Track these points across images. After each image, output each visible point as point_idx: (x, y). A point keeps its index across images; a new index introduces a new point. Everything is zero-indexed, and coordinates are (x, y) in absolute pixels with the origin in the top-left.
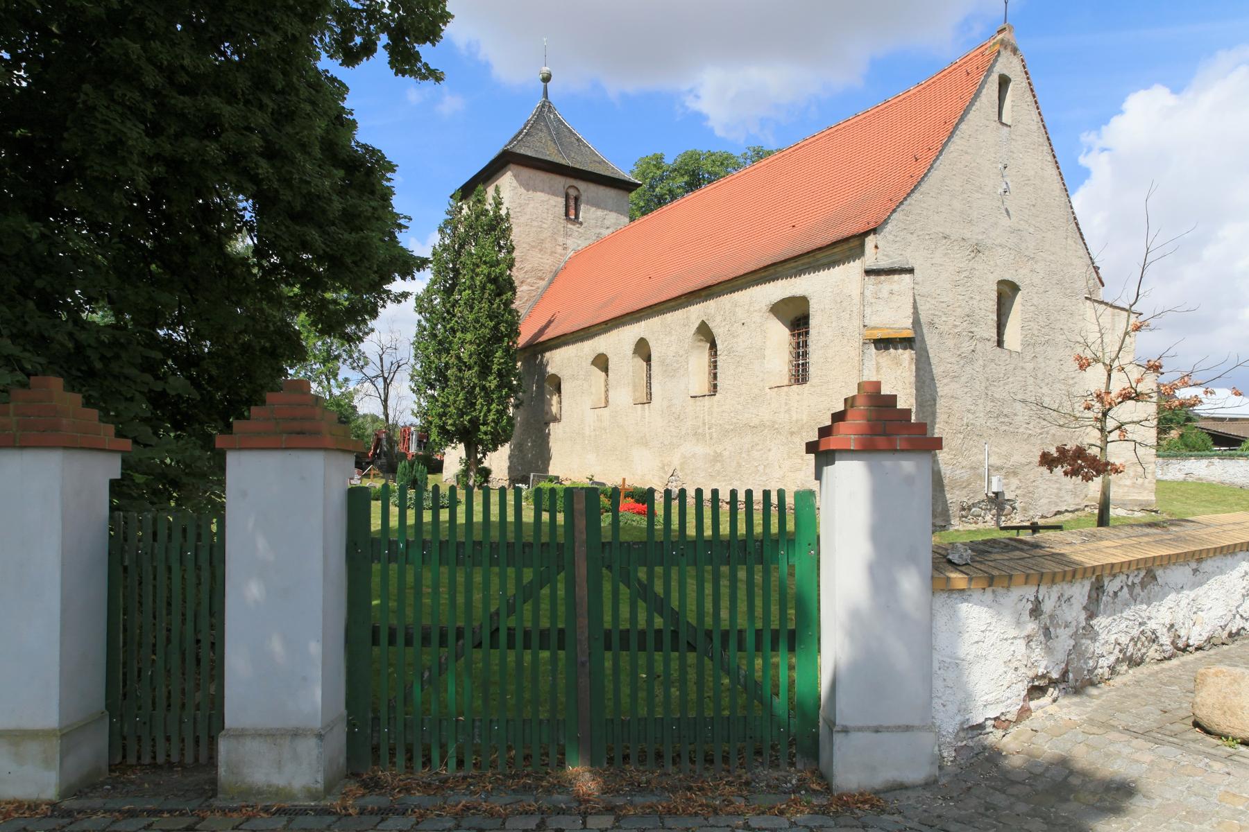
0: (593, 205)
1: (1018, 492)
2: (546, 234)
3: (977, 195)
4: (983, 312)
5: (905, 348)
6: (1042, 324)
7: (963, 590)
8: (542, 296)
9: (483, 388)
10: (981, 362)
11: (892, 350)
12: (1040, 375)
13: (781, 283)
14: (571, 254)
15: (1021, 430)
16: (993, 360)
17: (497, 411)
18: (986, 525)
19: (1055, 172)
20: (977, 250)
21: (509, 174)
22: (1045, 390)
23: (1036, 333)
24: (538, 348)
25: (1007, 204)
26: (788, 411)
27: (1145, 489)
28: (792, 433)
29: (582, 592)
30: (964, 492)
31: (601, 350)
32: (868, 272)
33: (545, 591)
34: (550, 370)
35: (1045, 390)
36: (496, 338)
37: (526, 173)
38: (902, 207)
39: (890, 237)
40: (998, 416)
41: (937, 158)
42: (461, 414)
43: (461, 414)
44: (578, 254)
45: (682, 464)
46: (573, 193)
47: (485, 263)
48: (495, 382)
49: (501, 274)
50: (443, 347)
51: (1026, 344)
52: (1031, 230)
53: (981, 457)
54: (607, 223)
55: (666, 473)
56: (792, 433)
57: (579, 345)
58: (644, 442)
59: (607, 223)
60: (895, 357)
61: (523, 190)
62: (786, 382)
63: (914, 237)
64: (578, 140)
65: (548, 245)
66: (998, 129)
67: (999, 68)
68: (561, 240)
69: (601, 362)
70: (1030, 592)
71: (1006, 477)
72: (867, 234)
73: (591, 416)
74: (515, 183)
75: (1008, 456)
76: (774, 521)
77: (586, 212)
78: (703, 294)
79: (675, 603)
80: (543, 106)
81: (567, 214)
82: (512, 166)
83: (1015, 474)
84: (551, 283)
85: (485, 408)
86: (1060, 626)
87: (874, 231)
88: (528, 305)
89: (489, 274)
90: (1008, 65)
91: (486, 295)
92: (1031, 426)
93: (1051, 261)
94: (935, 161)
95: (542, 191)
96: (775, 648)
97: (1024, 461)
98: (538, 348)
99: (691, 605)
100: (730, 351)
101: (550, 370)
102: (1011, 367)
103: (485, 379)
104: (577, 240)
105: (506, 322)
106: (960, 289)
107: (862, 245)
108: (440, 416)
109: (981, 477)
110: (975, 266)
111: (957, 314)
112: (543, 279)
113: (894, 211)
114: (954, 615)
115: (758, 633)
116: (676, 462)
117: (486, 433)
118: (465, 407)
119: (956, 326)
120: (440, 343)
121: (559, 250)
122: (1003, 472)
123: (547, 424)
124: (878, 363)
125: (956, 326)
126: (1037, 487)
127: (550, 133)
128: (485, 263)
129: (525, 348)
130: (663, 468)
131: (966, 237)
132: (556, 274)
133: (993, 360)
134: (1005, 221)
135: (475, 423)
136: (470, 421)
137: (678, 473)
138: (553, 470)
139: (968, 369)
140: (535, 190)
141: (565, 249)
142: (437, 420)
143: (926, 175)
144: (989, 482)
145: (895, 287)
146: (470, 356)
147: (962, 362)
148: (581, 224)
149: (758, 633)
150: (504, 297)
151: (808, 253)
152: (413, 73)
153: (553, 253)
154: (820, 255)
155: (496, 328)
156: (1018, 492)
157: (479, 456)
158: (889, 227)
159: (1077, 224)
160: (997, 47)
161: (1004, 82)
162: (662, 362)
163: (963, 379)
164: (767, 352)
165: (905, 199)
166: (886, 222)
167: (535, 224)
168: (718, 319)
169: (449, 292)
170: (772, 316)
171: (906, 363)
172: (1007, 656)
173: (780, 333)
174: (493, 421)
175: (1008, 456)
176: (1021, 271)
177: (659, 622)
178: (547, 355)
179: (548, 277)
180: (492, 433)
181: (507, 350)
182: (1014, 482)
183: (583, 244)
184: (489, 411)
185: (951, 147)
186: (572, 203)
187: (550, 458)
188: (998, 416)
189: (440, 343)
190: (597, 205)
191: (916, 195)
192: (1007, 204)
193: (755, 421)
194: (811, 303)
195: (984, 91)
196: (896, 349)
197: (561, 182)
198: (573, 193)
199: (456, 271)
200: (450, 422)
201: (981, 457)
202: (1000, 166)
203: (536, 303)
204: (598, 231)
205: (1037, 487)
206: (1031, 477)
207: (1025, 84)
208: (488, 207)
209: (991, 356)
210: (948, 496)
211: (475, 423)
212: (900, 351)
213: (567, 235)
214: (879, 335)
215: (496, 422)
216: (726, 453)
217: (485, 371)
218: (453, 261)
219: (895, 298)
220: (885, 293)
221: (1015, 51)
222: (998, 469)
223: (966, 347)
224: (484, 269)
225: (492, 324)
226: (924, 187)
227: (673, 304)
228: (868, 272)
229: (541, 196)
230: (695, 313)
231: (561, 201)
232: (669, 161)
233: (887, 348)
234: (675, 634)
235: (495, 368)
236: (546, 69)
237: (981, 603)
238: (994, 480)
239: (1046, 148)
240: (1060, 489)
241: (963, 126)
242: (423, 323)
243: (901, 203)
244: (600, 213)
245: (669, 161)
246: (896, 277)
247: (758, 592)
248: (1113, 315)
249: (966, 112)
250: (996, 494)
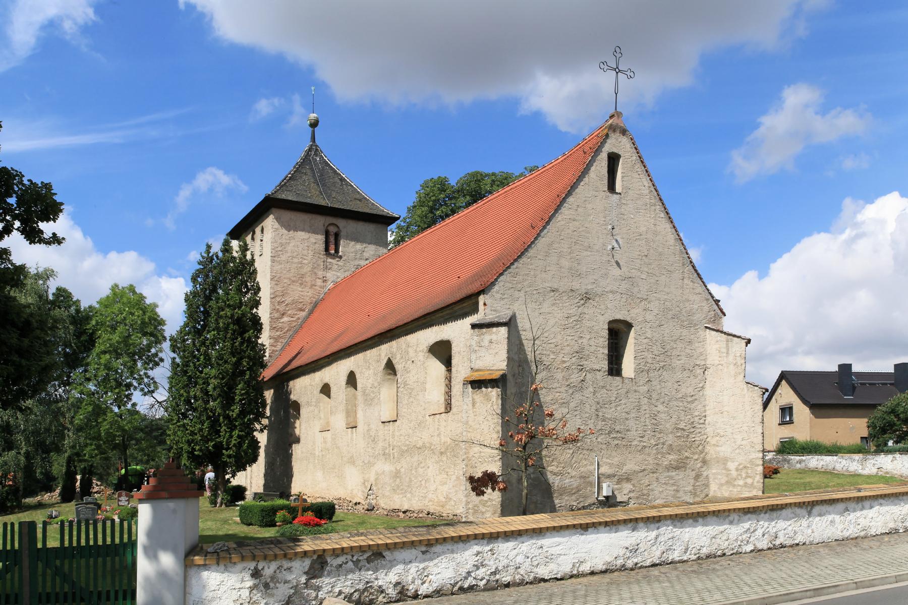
0: (352, 240)
1: (631, 495)
2: (306, 269)
3: (586, 253)
4: (593, 349)
5: (493, 387)
6: (656, 353)
7: (199, 565)
8: (301, 326)
9: (227, 417)
10: (591, 389)
11: (483, 389)
12: (655, 396)
13: (435, 329)
14: (330, 285)
15: (634, 443)
16: (603, 387)
17: (239, 437)
18: (731, 518)
19: (668, 226)
20: (587, 297)
21: (271, 217)
22: (661, 408)
23: (650, 361)
24: (283, 379)
25: (617, 257)
26: (439, 435)
27: (755, 488)
28: (442, 453)
29: (26, 573)
30: (574, 497)
31: (326, 380)
32: (474, 326)
33: (9, 576)
34: (293, 397)
35: (661, 408)
36: (237, 373)
37: (288, 215)
38: (510, 270)
39: (498, 296)
40: (610, 433)
41: (544, 227)
42: (206, 440)
43: (206, 440)
44: (337, 285)
45: (376, 479)
46: (333, 230)
47: (229, 306)
48: (237, 411)
49: (243, 315)
50: (191, 382)
51: (639, 371)
52: (644, 276)
53: (592, 468)
54: (366, 255)
55: (366, 487)
56: (442, 453)
57: (312, 375)
58: (352, 461)
59: (366, 255)
60: (486, 394)
61: (284, 231)
62: (443, 410)
63: (522, 294)
64: (342, 180)
65: (308, 279)
66: (607, 197)
67: (608, 148)
68: (320, 274)
69: (326, 390)
70: (252, 565)
71: (618, 483)
72: (479, 293)
73: (319, 437)
74: (277, 225)
75: (621, 465)
76: (126, 536)
77: (347, 247)
78: (389, 335)
79: (58, 579)
80: (310, 150)
81: (327, 249)
82: (273, 210)
83: (628, 480)
84: (311, 312)
85: (228, 434)
86: (280, 583)
87: (482, 292)
88: (288, 335)
89: (232, 315)
90: (617, 144)
91: (229, 335)
92: (645, 439)
93: (665, 300)
94: (541, 231)
95: (303, 231)
96: (125, 599)
97: (637, 468)
98: (283, 379)
99: (83, 579)
100: (405, 384)
101: (293, 397)
102: (623, 391)
103: (229, 409)
104: (337, 272)
105: (249, 357)
106: (568, 331)
107: (477, 304)
108: (189, 443)
109: (591, 484)
110: (586, 310)
111: (566, 352)
112: (304, 310)
113: (501, 274)
114: (200, 578)
115: (108, 592)
116: (372, 479)
117: (229, 456)
118: (209, 434)
119: (564, 362)
120: (190, 378)
121: (319, 282)
122: (588, 480)
123: (290, 446)
124: (473, 399)
125: (564, 362)
126: (652, 490)
127: (314, 176)
128: (229, 306)
129: (273, 378)
130: (364, 483)
131: (574, 288)
132: (316, 305)
133: (603, 387)
134: (616, 271)
135: (219, 447)
136: (214, 446)
137: (374, 488)
138: (295, 488)
139: (578, 396)
140: (296, 230)
141: (325, 281)
142: (186, 447)
143: (533, 243)
144: (600, 488)
145: (494, 337)
146: (214, 389)
147: (571, 391)
148: (341, 257)
149: (116, 592)
150: (247, 335)
151: (448, 306)
152: (40, 242)
153: (313, 286)
154: (456, 308)
155: (238, 364)
156: (631, 495)
157: (227, 477)
158: (496, 288)
159: (693, 267)
160: (605, 132)
161: (613, 160)
162: (364, 392)
163: (572, 405)
164: (428, 386)
165: (512, 264)
166: (493, 284)
167: (296, 260)
168: (398, 356)
169: (199, 333)
170: (431, 356)
171: (494, 399)
172: (235, 598)
173: (437, 367)
174: (234, 445)
175: (621, 465)
176: (632, 311)
177: (67, 588)
178: (291, 383)
179: (308, 308)
180: (234, 457)
181: (248, 383)
182: (627, 487)
183: (341, 275)
184: (231, 437)
185: (559, 217)
186: (332, 239)
187: (292, 476)
188: (610, 433)
189: (190, 378)
190: (356, 239)
191: (524, 259)
192: (617, 257)
193: (420, 444)
194: (453, 345)
195: (593, 168)
196: (486, 388)
197: (321, 221)
198: (333, 230)
199: (206, 313)
200: (197, 448)
201: (592, 468)
202: (610, 227)
203: (296, 332)
204: (357, 263)
205: (652, 490)
206: (646, 481)
207: (635, 157)
208: (235, 254)
209: (601, 384)
210: (556, 501)
211: (219, 447)
212: (490, 389)
213: (326, 268)
214: (476, 376)
215: (239, 445)
216: (402, 470)
217: (228, 399)
218: (204, 306)
219: (493, 346)
220: (486, 343)
221: (624, 132)
222: (609, 476)
223: (575, 378)
224: (228, 312)
225: (234, 360)
226: (531, 252)
227: (370, 343)
228: (474, 326)
229: (301, 235)
230: (384, 351)
231: (321, 238)
232: (453, 182)
233: (480, 388)
234: (74, 594)
235: (237, 398)
236: (313, 116)
237: (217, 571)
238: (605, 485)
239: (659, 207)
240: (677, 491)
241: (571, 199)
242: (178, 360)
243: (509, 267)
244: (359, 246)
245: (453, 182)
246: (495, 329)
247: (92, 569)
248: (727, 341)
249: (574, 187)
250: (607, 497)
